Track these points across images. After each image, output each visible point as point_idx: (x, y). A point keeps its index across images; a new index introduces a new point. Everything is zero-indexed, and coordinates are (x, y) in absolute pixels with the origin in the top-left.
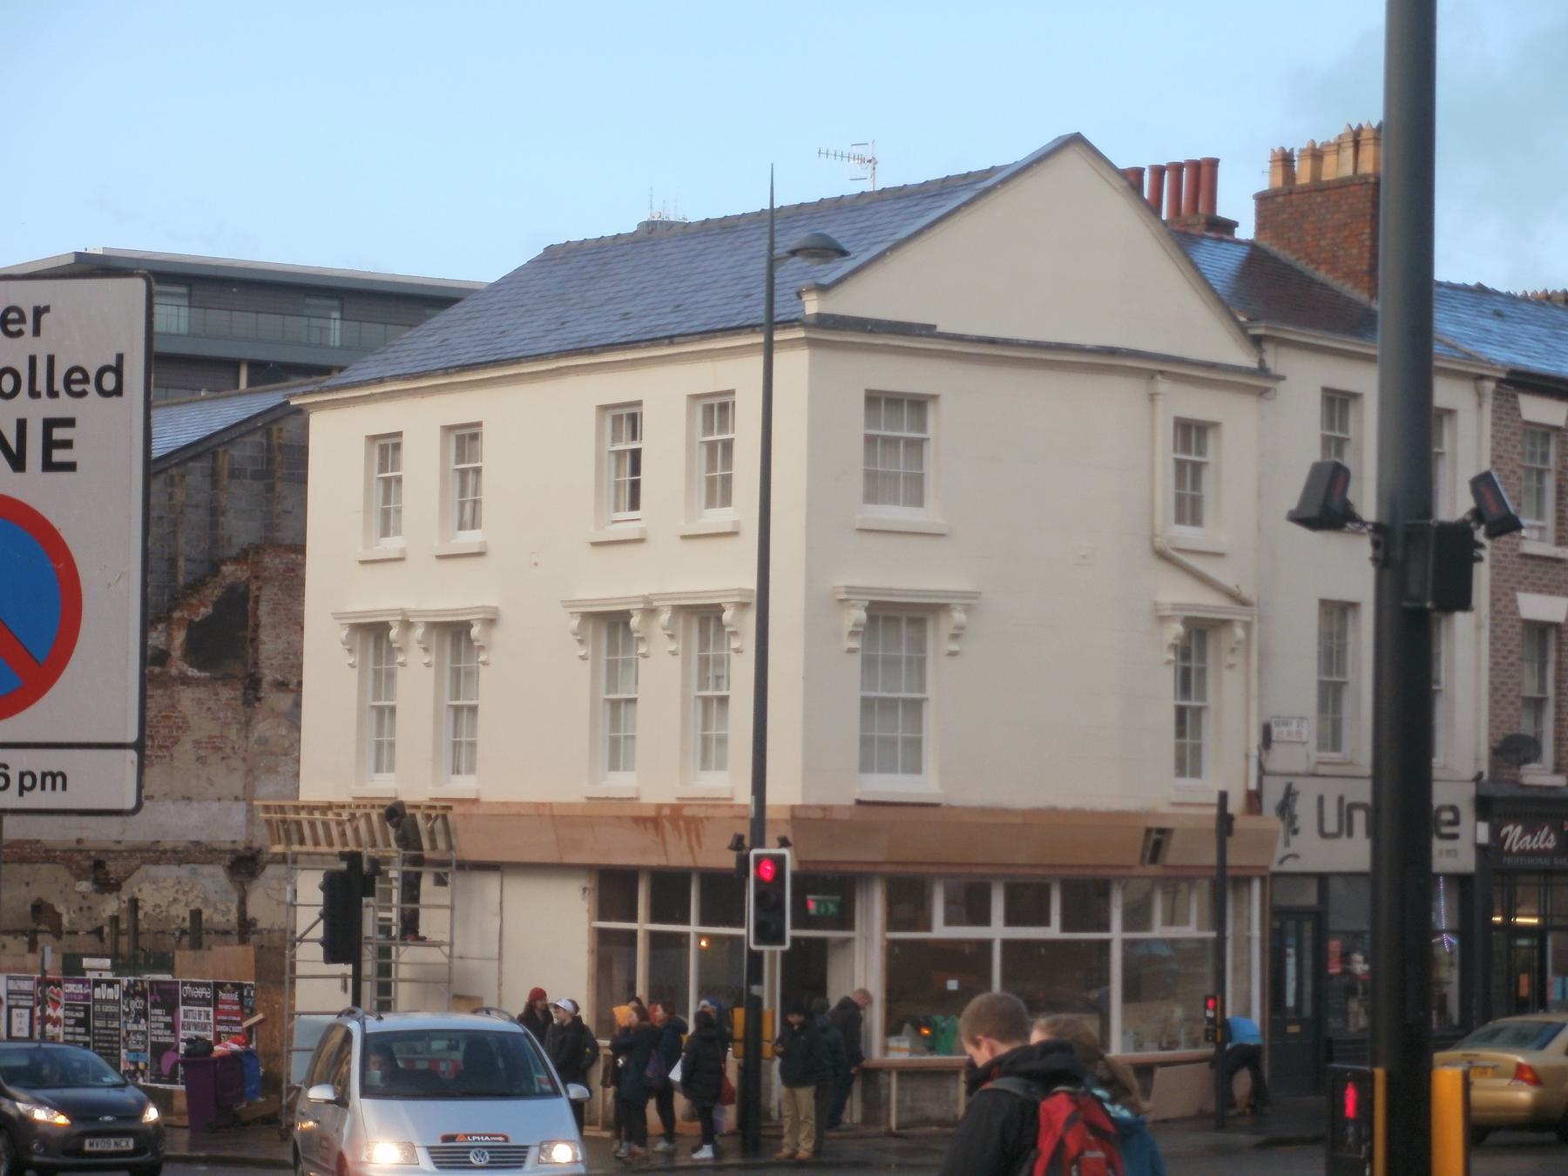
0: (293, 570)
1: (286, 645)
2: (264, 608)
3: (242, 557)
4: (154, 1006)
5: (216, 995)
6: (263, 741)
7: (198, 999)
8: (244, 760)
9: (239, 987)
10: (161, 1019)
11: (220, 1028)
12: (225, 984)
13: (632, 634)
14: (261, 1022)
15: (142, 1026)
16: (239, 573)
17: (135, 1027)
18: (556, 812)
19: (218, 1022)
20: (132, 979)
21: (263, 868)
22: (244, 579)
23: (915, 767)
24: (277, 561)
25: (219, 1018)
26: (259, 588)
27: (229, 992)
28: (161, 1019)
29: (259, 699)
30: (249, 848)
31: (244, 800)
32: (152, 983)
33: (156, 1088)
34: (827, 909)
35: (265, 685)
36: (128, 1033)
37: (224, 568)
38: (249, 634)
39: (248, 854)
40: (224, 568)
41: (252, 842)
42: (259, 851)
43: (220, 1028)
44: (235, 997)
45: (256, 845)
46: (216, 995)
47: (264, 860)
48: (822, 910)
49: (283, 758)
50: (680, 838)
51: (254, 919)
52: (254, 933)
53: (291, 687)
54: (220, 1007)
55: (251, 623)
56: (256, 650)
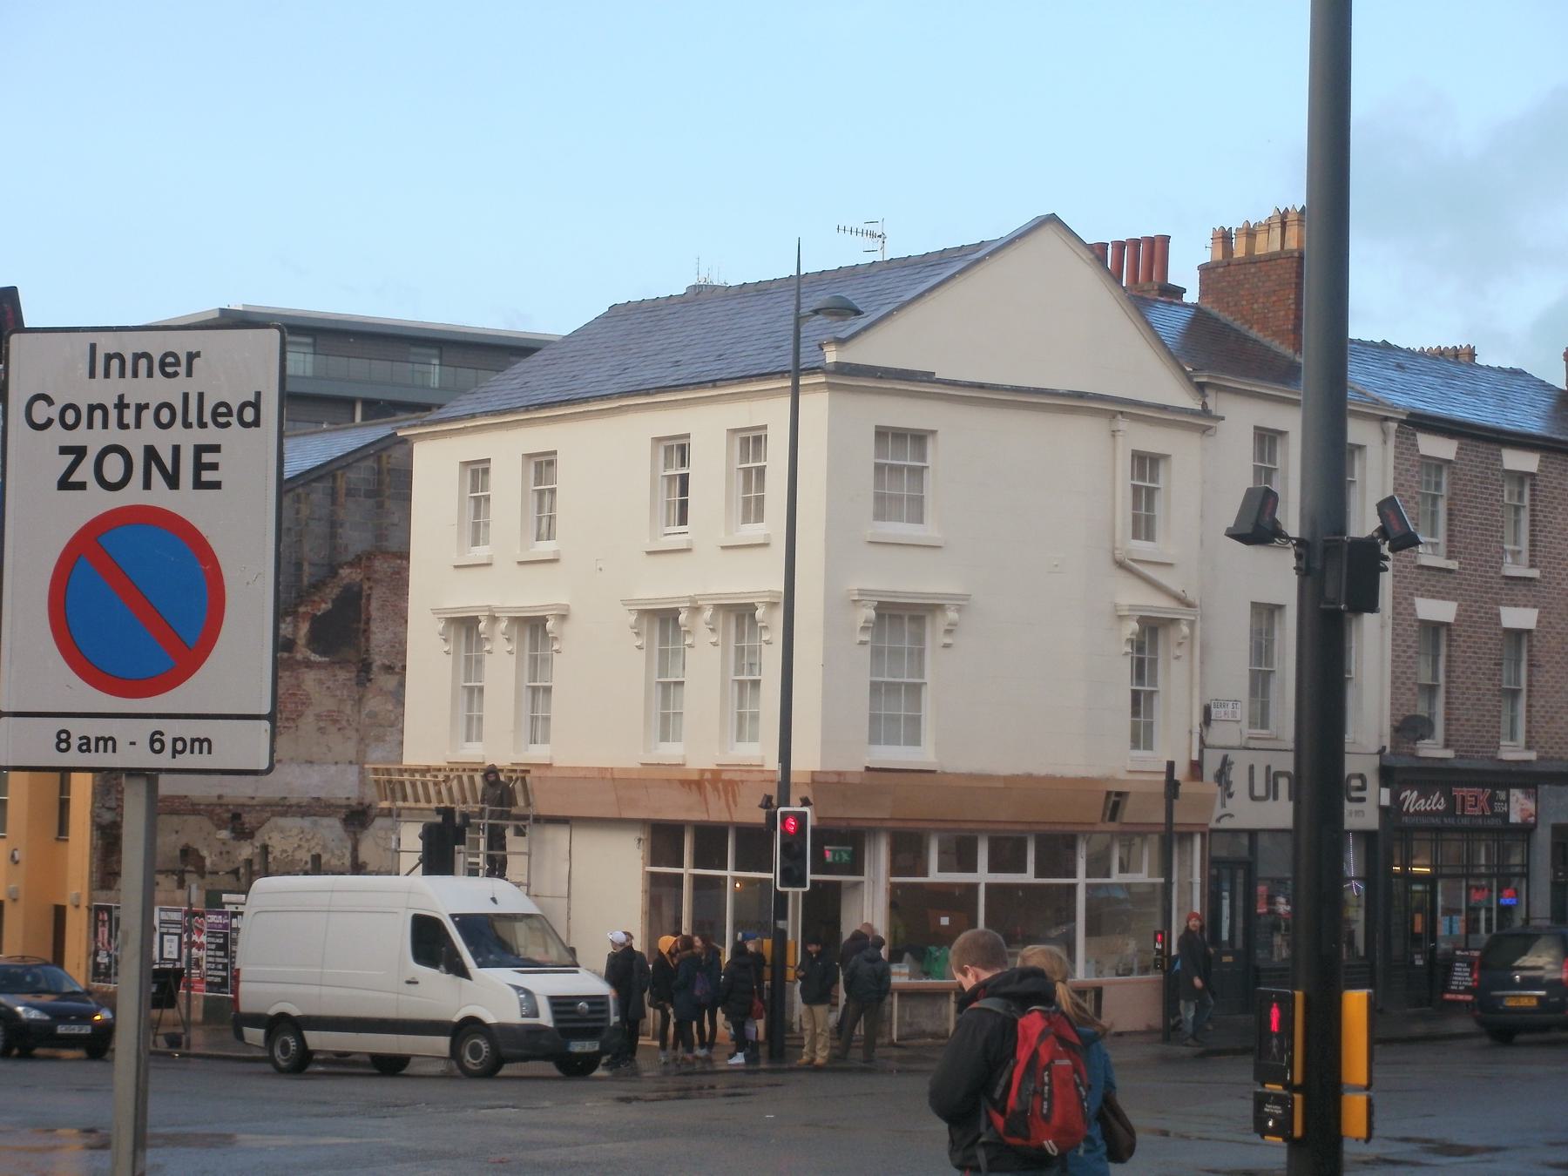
1: (393, 636)
2: (374, 604)
3: (355, 563)
6: (372, 715)
8: (357, 730)
16: (354, 576)
22: (358, 580)
23: (914, 740)
24: (386, 565)
26: (370, 588)
29: (370, 680)
30: (361, 804)
31: (357, 764)
34: (840, 859)
35: (375, 668)
37: (341, 571)
38: (362, 626)
39: (360, 808)
40: (341, 571)
41: (363, 798)
48: (837, 858)
55: (363, 617)
56: (368, 640)
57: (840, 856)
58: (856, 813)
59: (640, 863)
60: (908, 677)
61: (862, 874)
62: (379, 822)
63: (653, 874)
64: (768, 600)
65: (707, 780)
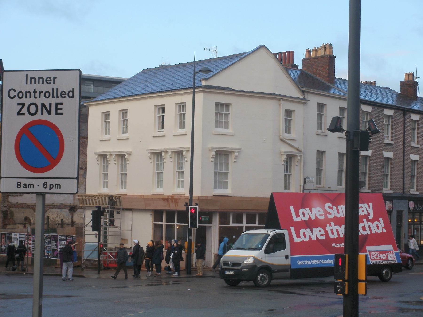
0: (84, 142)
4: (53, 240)
5: (67, 238)
7: (63, 239)
9: (72, 236)
10: (54, 243)
12: (69, 236)
13: (183, 156)
15: (50, 245)
17: (48, 245)
18: (145, 197)
20: (47, 234)
21: (77, 210)
27: (69, 237)
28: (54, 243)
30: (74, 205)
32: (52, 235)
33: (53, 259)
34: (206, 220)
36: (47, 247)
39: (74, 206)
41: (74, 204)
42: (76, 206)
44: (71, 239)
45: (75, 204)
46: (67, 238)
47: (77, 208)
49: (82, 185)
51: (75, 221)
53: (83, 169)
57: (206, 219)
59: (151, 221)
61: (212, 224)
62: (79, 210)
64: (109, 153)
65: (170, 198)
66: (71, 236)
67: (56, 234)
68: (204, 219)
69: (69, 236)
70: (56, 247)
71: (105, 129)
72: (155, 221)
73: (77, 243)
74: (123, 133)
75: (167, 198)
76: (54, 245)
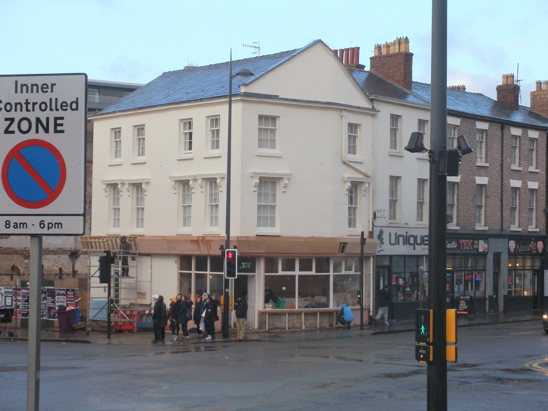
4: (49, 296)
9: (73, 290)
10: (50, 300)
11: (68, 302)
14: (80, 300)
18: (168, 239)
19: (67, 301)
25: (68, 299)
27: (70, 292)
28: (50, 300)
32: (48, 289)
41: (76, 248)
42: (78, 251)
43: (68, 302)
44: (72, 293)
48: (246, 267)
50: (205, 246)
51: (77, 271)
52: (77, 274)
54: (68, 296)
57: (247, 266)
58: (252, 251)
60: (264, 203)
62: (82, 256)
63: (181, 274)
65: (200, 240)
66: (72, 290)
67: (52, 288)
68: (245, 266)
69: (70, 290)
70: (52, 304)
71: (114, 151)
72: (181, 270)
73: (80, 299)
74: (138, 156)
75: (196, 239)
76: (51, 302)
